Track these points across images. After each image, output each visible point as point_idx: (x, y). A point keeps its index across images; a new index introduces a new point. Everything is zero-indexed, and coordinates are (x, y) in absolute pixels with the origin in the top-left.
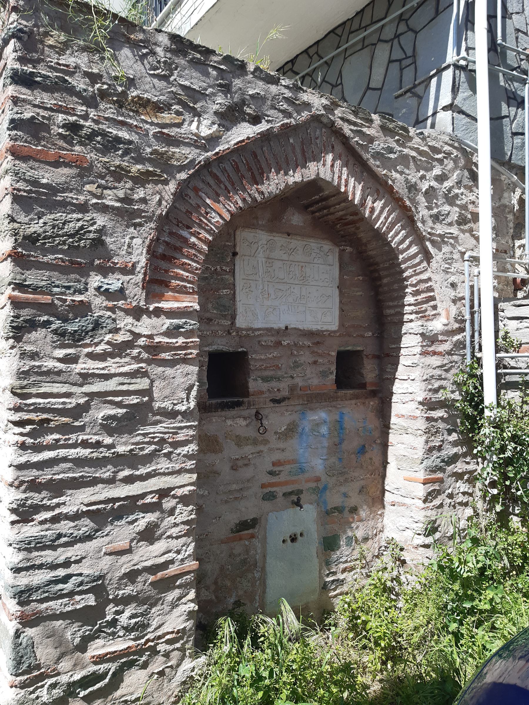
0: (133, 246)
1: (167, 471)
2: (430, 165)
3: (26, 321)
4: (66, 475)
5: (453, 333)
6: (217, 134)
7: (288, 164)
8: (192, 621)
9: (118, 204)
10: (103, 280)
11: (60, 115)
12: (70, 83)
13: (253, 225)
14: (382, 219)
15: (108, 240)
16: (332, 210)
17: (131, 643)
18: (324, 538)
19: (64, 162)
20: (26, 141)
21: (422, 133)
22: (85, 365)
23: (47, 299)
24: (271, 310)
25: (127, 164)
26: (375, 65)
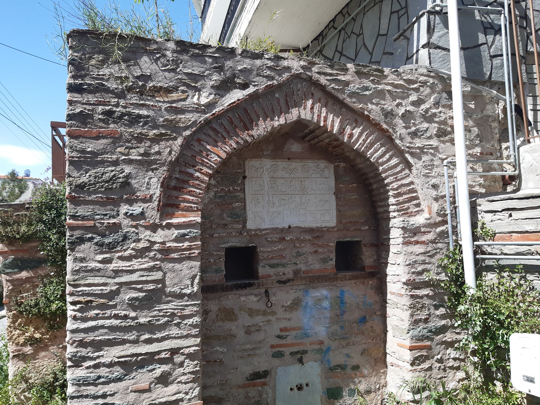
0: (151, 184)
2: (405, 94)
3: (77, 238)
4: (104, 337)
5: (436, 225)
6: (214, 101)
7: (274, 112)
9: (140, 158)
10: (129, 208)
11: (100, 107)
14: (361, 141)
15: (133, 182)
18: (328, 389)
19: (102, 136)
20: (78, 127)
21: (397, 71)
22: (117, 264)
23: (91, 223)
25: (146, 131)
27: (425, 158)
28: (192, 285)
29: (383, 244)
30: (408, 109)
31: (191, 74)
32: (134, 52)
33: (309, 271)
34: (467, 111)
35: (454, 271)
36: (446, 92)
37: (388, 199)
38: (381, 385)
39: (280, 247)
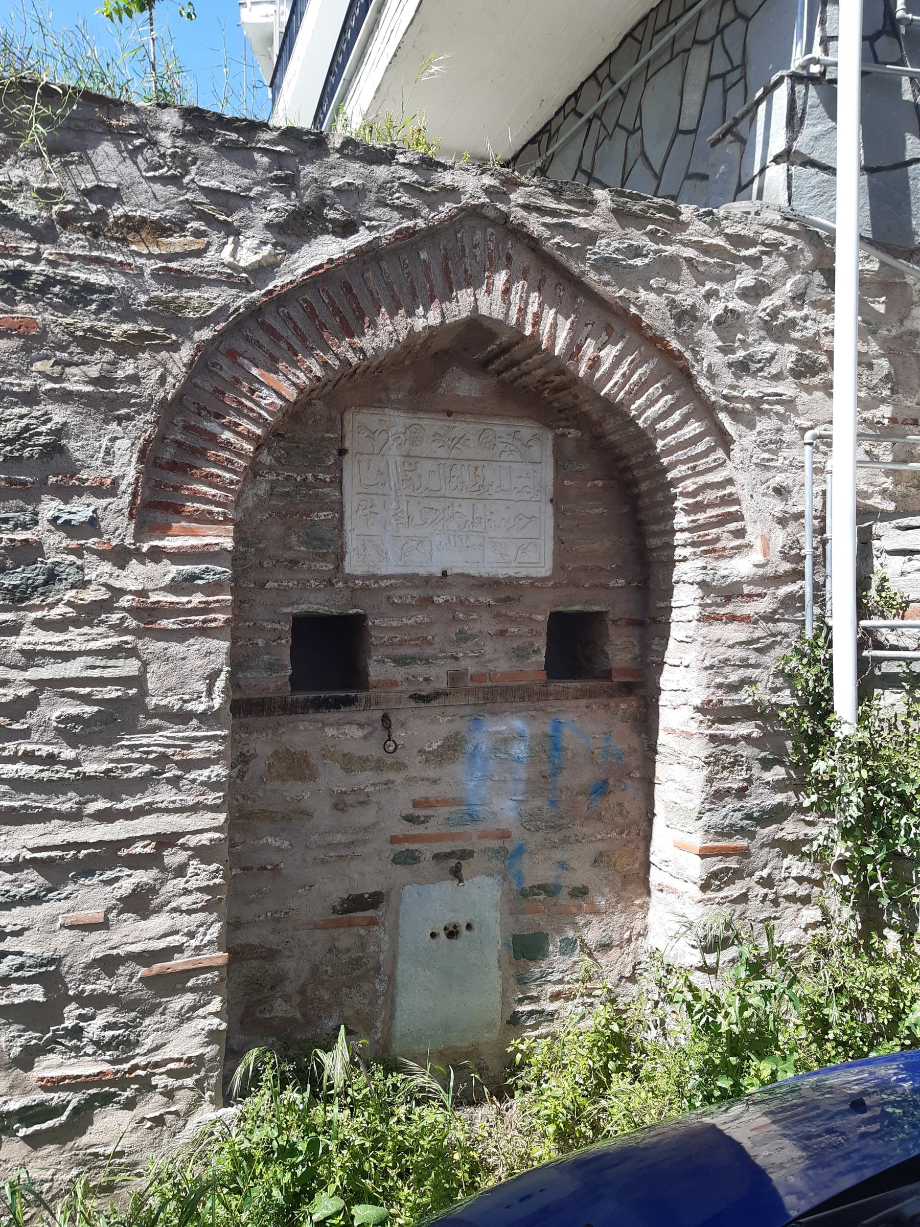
0: (115, 453)
1: (171, 806)
2: (727, 271)
5: (778, 579)
6: (272, 260)
7: (414, 296)
8: (216, 1047)
10: (62, 507)
12: (10, 210)
13: (380, 401)
14: (617, 377)
15: (72, 445)
16: (523, 366)
17: (106, 1067)
18: (515, 937)
21: (710, 213)
24: (415, 544)
25: (105, 325)
26: (687, 88)
27: (763, 424)
28: (210, 693)
29: (655, 621)
30: (731, 305)
31: (218, 191)
32: (80, 131)
33: (484, 675)
34: (867, 318)
35: (811, 684)
36: (822, 271)
37: (672, 516)
38: (635, 932)
39: (420, 618)
